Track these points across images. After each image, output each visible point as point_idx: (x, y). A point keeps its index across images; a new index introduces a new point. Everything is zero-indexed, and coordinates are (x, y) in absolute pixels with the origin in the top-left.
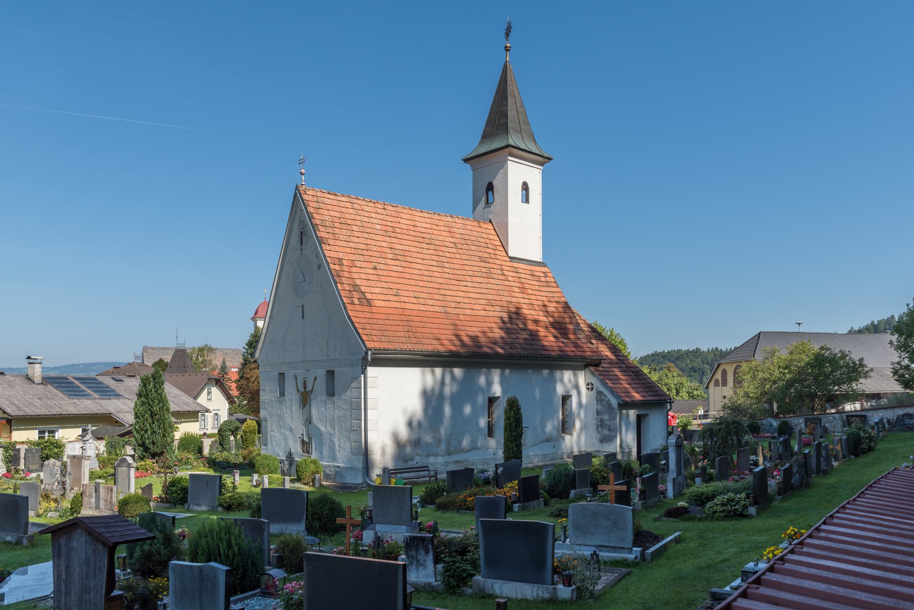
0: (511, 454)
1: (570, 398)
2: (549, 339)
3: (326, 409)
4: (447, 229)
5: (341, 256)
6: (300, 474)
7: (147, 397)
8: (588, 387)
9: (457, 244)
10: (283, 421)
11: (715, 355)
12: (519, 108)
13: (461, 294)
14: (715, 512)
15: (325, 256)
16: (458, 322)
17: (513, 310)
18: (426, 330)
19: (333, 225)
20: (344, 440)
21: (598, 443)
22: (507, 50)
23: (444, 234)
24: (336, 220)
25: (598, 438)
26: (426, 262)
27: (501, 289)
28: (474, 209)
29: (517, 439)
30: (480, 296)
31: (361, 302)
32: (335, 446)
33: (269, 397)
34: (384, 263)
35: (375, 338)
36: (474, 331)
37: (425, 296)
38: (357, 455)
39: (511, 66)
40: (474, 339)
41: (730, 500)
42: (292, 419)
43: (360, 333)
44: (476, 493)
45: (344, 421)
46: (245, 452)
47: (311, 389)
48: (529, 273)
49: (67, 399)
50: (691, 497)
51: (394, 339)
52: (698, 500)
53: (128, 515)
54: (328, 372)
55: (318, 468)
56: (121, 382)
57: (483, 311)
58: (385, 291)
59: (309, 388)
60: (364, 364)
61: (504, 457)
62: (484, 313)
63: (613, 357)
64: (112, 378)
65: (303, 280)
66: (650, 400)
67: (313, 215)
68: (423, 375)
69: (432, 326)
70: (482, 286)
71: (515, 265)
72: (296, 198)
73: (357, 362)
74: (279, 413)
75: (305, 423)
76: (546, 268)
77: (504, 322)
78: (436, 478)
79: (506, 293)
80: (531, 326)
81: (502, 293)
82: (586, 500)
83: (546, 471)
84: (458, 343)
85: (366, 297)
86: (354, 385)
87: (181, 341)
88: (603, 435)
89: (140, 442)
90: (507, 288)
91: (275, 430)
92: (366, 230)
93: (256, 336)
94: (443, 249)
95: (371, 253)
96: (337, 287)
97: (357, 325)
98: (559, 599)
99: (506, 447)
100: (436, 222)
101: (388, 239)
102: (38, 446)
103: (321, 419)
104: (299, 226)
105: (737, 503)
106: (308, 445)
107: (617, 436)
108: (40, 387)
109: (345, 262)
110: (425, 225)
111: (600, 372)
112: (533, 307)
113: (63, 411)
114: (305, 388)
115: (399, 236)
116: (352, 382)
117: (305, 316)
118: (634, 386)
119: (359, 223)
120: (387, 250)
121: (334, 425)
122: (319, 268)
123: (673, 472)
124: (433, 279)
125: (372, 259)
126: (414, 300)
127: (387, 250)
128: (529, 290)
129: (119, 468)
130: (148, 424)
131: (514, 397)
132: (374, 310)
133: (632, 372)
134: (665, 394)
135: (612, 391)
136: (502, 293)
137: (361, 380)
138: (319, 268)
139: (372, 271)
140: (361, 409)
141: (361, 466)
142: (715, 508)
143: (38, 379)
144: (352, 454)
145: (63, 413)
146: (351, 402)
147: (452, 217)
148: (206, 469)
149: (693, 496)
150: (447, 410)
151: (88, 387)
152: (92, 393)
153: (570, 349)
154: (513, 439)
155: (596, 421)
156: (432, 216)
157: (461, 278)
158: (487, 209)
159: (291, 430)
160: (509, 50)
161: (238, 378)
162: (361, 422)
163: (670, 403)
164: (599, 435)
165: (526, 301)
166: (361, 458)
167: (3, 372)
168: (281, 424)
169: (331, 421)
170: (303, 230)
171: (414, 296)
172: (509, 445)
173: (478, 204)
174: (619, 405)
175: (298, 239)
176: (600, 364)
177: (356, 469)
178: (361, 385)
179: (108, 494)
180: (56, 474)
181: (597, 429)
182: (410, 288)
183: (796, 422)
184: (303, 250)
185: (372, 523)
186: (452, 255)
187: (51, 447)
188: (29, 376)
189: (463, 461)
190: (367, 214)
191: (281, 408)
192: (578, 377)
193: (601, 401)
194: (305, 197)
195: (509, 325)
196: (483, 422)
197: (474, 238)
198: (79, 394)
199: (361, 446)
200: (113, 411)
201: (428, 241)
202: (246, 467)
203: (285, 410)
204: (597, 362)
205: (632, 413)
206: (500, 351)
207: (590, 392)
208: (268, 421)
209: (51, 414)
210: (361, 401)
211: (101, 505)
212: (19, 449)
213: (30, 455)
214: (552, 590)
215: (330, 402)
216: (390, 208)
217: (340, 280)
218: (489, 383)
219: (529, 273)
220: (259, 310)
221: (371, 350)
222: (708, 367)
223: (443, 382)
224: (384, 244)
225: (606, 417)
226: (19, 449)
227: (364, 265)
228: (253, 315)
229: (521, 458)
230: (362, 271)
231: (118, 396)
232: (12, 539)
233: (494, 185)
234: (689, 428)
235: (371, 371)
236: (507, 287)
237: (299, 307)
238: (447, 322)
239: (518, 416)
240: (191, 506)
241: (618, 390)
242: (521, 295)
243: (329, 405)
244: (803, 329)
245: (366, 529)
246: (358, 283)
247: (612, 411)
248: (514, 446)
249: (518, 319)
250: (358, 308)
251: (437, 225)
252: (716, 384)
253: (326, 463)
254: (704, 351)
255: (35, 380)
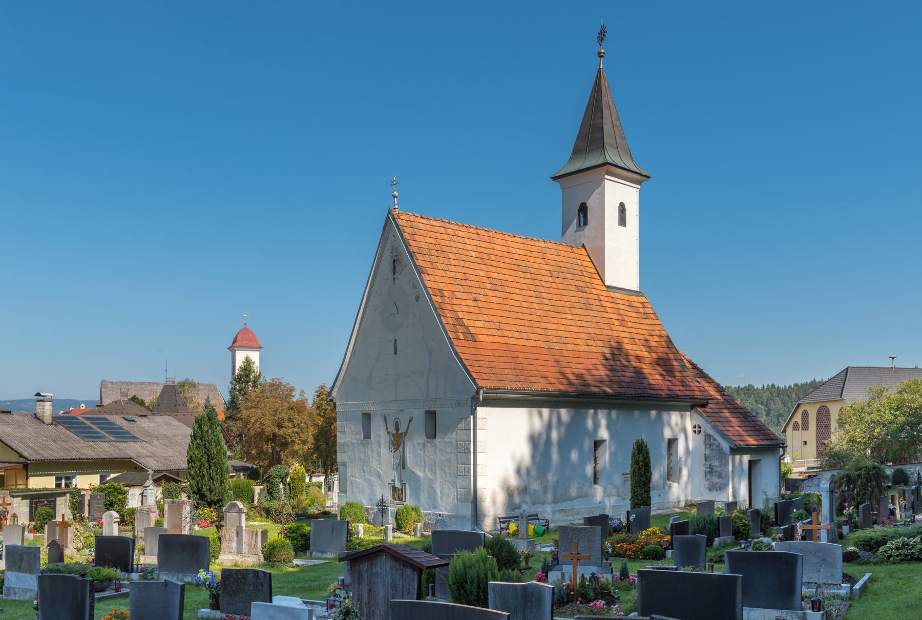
0: (639, 501)
1: (676, 442)
2: (655, 377)
3: (424, 452)
4: (540, 255)
5: (441, 286)
6: (401, 522)
7: (203, 439)
8: (695, 429)
10: (367, 465)
11: (771, 393)
12: (614, 121)
13: (562, 328)
14: (889, 557)
15: (425, 287)
16: (562, 359)
17: (614, 345)
18: (533, 367)
19: (430, 252)
20: (449, 487)
21: (707, 492)
23: (539, 261)
24: (432, 247)
25: (707, 486)
26: (524, 292)
28: (563, 234)
30: (581, 330)
31: (466, 337)
32: (435, 492)
33: (350, 440)
35: (485, 376)
36: (579, 369)
37: (527, 329)
38: (465, 502)
39: (605, 75)
40: (579, 377)
41: (905, 545)
42: (380, 463)
44: (624, 539)
45: (448, 466)
49: (81, 441)
50: (859, 542)
51: (502, 377)
52: (867, 545)
53: (275, 559)
54: (427, 412)
55: (419, 515)
56: (133, 422)
57: (585, 346)
60: (474, 404)
62: (587, 349)
63: (719, 397)
64: (123, 418)
66: (763, 445)
67: (409, 242)
68: (531, 417)
70: (582, 318)
71: (612, 294)
72: (389, 222)
73: (465, 402)
74: (362, 457)
75: (397, 468)
77: (606, 359)
78: (548, 528)
79: (606, 326)
80: (636, 364)
81: (603, 326)
82: (741, 546)
84: (564, 381)
86: (462, 425)
87: (170, 375)
88: (713, 482)
89: (195, 489)
91: (357, 475)
92: (463, 257)
93: (246, 370)
95: (469, 283)
99: (634, 493)
100: (529, 247)
101: (484, 267)
102: (101, 492)
103: (419, 463)
105: (913, 547)
106: (400, 492)
107: (729, 484)
108: (51, 427)
109: (446, 294)
110: (519, 251)
111: (708, 414)
112: (634, 341)
113: (81, 455)
114: (397, 430)
115: (495, 264)
116: (459, 423)
118: (745, 429)
120: (485, 280)
121: (435, 470)
123: (827, 519)
124: (533, 311)
125: (471, 290)
126: (517, 335)
127: (485, 280)
129: (228, 514)
130: (205, 469)
131: (642, 440)
132: (479, 345)
133: (740, 413)
135: (724, 435)
136: (603, 326)
137: (470, 421)
138: (417, 300)
139: (472, 303)
140: (470, 453)
142: (889, 552)
143: (48, 419)
144: (457, 501)
145: (81, 457)
146: (457, 444)
148: (263, 519)
149: (860, 541)
150: (555, 456)
151: (102, 428)
152: (106, 435)
153: (678, 389)
154: (642, 485)
155: (704, 467)
156: (525, 241)
157: (560, 309)
159: (379, 475)
160: (602, 56)
161: (224, 419)
163: (783, 447)
164: (707, 483)
165: (627, 335)
166: (469, 505)
167: (10, 410)
168: (365, 469)
169: (431, 465)
170: (396, 258)
171: (516, 330)
173: (569, 227)
174: (731, 449)
176: (707, 403)
177: (463, 517)
178: (470, 426)
179: (252, 538)
180: (186, 518)
181: (706, 476)
182: (511, 321)
183: (912, 470)
184: (396, 279)
185: (558, 564)
186: (548, 285)
187: (115, 493)
188: (38, 415)
190: (461, 240)
192: (685, 419)
193: (710, 445)
194: (399, 222)
195: (612, 362)
196: (589, 470)
198: (93, 436)
199: (470, 492)
200: (133, 456)
201: (523, 269)
202: (302, 518)
205: (746, 458)
206: (608, 390)
207: (697, 435)
208: (348, 465)
209: (69, 458)
210: (469, 444)
211: (244, 549)
212: (84, 495)
213: (94, 502)
214: (802, 615)
216: (483, 232)
217: (444, 313)
218: (597, 426)
219: (627, 303)
220: (238, 338)
221: (482, 388)
222: (763, 407)
223: (549, 427)
224: (481, 273)
225: (716, 463)
226: (84, 495)
227: (464, 296)
228: (230, 344)
229: (649, 505)
230: (463, 302)
231: (134, 438)
232: (193, 579)
233: (587, 206)
235: (481, 411)
236: (606, 320)
237: (390, 341)
238: (551, 358)
239: (647, 460)
240: (314, 553)
241: (728, 433)
242: (621, 329)
243: (429, 448)
244: (898, 364)
245: (551, 571)
246: (461, 316)
247: (723, 456)
248: (643, 492)
249: (620, 355)
250: (464, 343)
251: (530, 251)
252: (796, 427)
253: (424, 511)
254: (757, 388)
255: (45, 420)
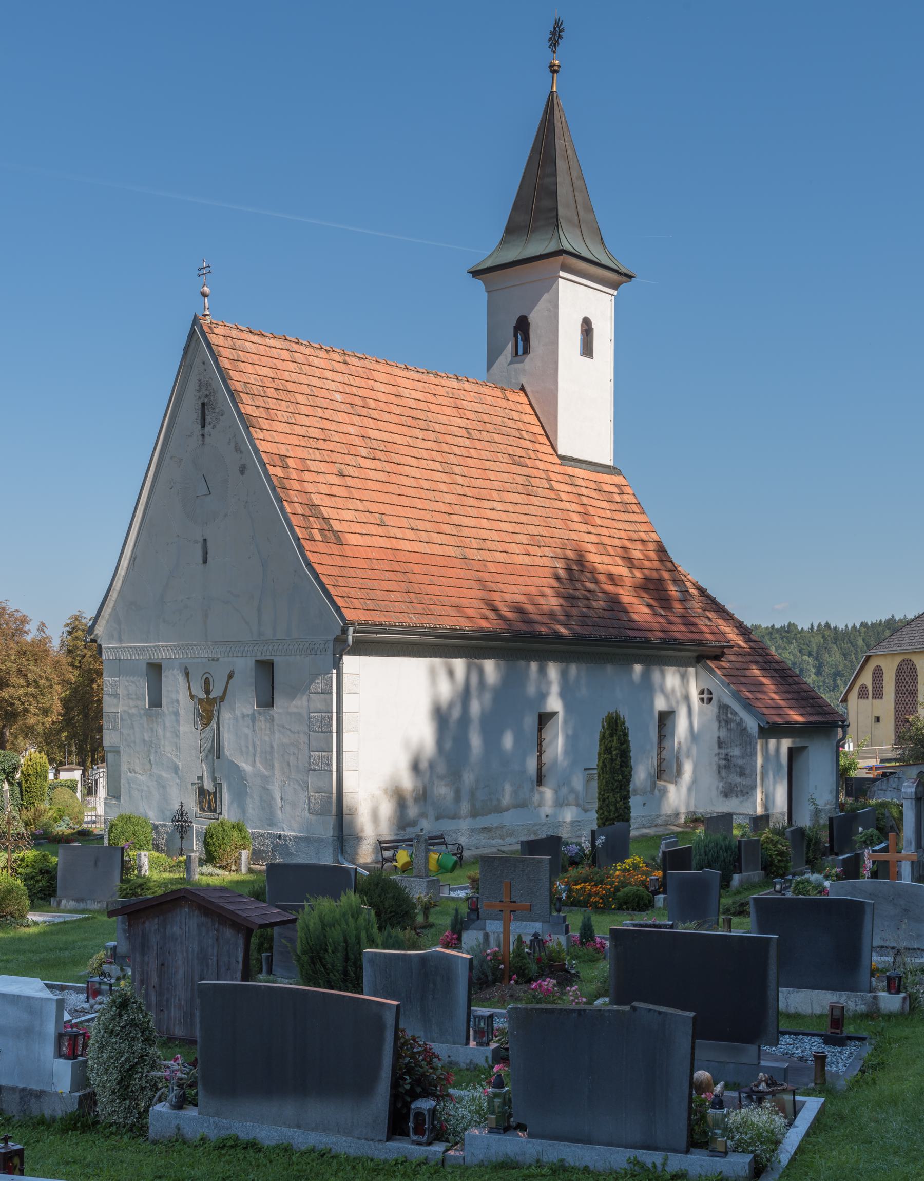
3: (254, 731)
5: (283, 450)
8: (702, 696)
9: (471, 431)
11: (823, 637)
13: (485, 524)
15: (257, 451)
16: (486, 576)
19: (265, 392)
20: (294, 788)
22: (554, 72)
23: (449, 411)
24: (268, 382)
25: (721, 789)
26: (423, 463)
27: (550, 515)
28: (490, 364)
29: (623, 788)
30: (518, 528)
32: (273, 798)
33: (126, 708)
34: (355, 464)
35: (357, 604)
37: (428, 526)
39: (562, 102)
42: (178, 748)
43: (332, 594)
45: (294, 754)
46: (29, 815)
47: (220, 694)
48: (594, 486)
54: (260, 663)
55: (245, 837)
58: (362, 517)
59: (215, 693)
61: (598, 819)
62: (526, 560)
65: (205, 491)
67: (228, 373)
68: (433, 673)
69: (445, 581)
70: (518, 508)
71: (570, 470)
72: (194, 339)
74: (147, 738)
76: (621, 477)
79: (559, 523)
81: (553, 523)
83: (666, 843)
85: (332, 527)
90: (559, 514)
91: (138, 769)
94: (449, 439)
95: (331, 446)
96: (282, 509)
97: (325, 580)
98: (883, 1012)
101: (356, 420)
103: (244, 749)
104: (199, 391)
107: (755, 786)
109: (291, 463)
112: (605, 549)
115: (374, 414)
117: (209, 560)
119: (307, 390)
120: (357, 441)
122: (243, 470)
123: (911, 843)
126: (410, 535)
127: (357, 441)
128: (596, 518)
131: (616, 713)
132: (348, 551)
133: (775, 670)
134: (833, 712)
135: (748, 706)
136: (553, 523)
137: (331, 679)
141: (331, 833)
146: (309, 718)
147: (457, 379)
153: (679, 631)
154: (617, 787)
156: (424, 377)
157: (484, 494)
158: (516, 366)
159: (176, 769)
160: (557, 72)
162: (332, 755)
163: (843, 727)
164: (721, 784)
165: (593, 538)
166: (331, 820)
168: (152, 758)
171: (409, 527)
172: (608, 798)
175: (195, 416)
176: (723, 654)
178: (331, 687)
181: (719, 772)
186: (464, 452)
189: (497, 828)
190: (318, 372)
191: (152, 729)
193: (727, 722)
194: (212, 338)
197: (498, 420)
199: (331, 798)
201: (423, 424)
203: (160, 731)
204: (718, 652)
206: (562, 630)
208: (122, 752)
210: (330, 718)
215: (262, 719)
217: (287, 495)
219: (594, 486)
221: (352, 624)
222: (810, 660)
224: (352, 430)
225: (736, 752)
227: (322, 467)
229: (628, 820)
230: (321, 478)
233: (530, 321)
234: (852, 774)
235: (350, 662)
236: (559, 512)
237: (196, 542)
238: (468, 575)
242: (584, 528)
243: (262, 723)
246: (317, 502)
250: (322, 547)
251: (434, 395)
252: (863, 694)
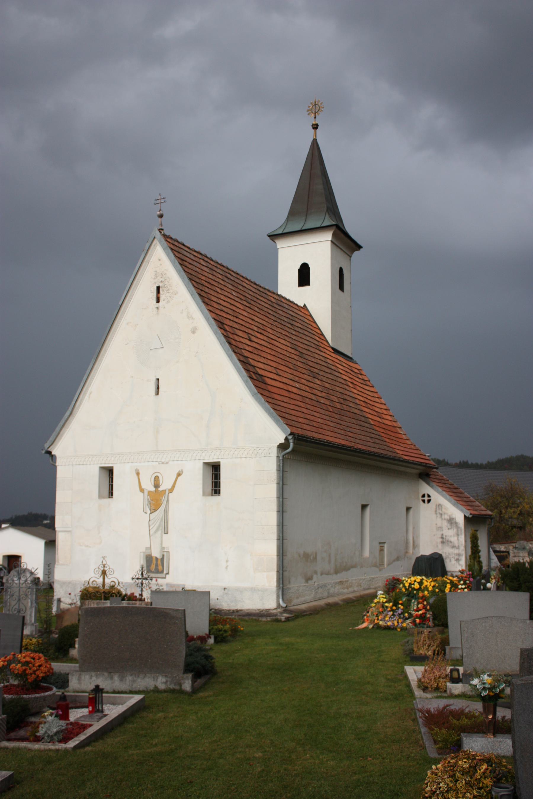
114: (157, 486)
138: (193, 332)
